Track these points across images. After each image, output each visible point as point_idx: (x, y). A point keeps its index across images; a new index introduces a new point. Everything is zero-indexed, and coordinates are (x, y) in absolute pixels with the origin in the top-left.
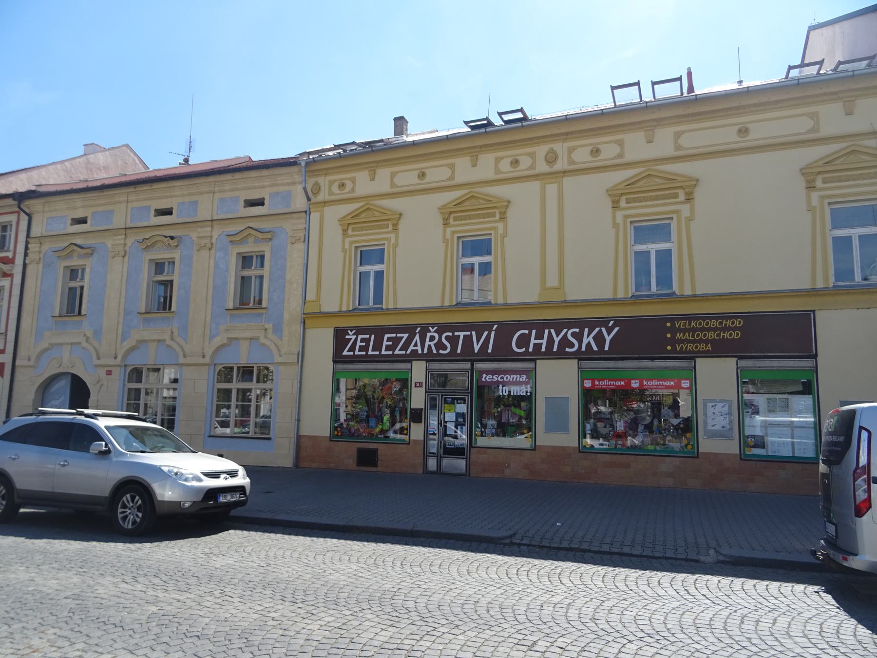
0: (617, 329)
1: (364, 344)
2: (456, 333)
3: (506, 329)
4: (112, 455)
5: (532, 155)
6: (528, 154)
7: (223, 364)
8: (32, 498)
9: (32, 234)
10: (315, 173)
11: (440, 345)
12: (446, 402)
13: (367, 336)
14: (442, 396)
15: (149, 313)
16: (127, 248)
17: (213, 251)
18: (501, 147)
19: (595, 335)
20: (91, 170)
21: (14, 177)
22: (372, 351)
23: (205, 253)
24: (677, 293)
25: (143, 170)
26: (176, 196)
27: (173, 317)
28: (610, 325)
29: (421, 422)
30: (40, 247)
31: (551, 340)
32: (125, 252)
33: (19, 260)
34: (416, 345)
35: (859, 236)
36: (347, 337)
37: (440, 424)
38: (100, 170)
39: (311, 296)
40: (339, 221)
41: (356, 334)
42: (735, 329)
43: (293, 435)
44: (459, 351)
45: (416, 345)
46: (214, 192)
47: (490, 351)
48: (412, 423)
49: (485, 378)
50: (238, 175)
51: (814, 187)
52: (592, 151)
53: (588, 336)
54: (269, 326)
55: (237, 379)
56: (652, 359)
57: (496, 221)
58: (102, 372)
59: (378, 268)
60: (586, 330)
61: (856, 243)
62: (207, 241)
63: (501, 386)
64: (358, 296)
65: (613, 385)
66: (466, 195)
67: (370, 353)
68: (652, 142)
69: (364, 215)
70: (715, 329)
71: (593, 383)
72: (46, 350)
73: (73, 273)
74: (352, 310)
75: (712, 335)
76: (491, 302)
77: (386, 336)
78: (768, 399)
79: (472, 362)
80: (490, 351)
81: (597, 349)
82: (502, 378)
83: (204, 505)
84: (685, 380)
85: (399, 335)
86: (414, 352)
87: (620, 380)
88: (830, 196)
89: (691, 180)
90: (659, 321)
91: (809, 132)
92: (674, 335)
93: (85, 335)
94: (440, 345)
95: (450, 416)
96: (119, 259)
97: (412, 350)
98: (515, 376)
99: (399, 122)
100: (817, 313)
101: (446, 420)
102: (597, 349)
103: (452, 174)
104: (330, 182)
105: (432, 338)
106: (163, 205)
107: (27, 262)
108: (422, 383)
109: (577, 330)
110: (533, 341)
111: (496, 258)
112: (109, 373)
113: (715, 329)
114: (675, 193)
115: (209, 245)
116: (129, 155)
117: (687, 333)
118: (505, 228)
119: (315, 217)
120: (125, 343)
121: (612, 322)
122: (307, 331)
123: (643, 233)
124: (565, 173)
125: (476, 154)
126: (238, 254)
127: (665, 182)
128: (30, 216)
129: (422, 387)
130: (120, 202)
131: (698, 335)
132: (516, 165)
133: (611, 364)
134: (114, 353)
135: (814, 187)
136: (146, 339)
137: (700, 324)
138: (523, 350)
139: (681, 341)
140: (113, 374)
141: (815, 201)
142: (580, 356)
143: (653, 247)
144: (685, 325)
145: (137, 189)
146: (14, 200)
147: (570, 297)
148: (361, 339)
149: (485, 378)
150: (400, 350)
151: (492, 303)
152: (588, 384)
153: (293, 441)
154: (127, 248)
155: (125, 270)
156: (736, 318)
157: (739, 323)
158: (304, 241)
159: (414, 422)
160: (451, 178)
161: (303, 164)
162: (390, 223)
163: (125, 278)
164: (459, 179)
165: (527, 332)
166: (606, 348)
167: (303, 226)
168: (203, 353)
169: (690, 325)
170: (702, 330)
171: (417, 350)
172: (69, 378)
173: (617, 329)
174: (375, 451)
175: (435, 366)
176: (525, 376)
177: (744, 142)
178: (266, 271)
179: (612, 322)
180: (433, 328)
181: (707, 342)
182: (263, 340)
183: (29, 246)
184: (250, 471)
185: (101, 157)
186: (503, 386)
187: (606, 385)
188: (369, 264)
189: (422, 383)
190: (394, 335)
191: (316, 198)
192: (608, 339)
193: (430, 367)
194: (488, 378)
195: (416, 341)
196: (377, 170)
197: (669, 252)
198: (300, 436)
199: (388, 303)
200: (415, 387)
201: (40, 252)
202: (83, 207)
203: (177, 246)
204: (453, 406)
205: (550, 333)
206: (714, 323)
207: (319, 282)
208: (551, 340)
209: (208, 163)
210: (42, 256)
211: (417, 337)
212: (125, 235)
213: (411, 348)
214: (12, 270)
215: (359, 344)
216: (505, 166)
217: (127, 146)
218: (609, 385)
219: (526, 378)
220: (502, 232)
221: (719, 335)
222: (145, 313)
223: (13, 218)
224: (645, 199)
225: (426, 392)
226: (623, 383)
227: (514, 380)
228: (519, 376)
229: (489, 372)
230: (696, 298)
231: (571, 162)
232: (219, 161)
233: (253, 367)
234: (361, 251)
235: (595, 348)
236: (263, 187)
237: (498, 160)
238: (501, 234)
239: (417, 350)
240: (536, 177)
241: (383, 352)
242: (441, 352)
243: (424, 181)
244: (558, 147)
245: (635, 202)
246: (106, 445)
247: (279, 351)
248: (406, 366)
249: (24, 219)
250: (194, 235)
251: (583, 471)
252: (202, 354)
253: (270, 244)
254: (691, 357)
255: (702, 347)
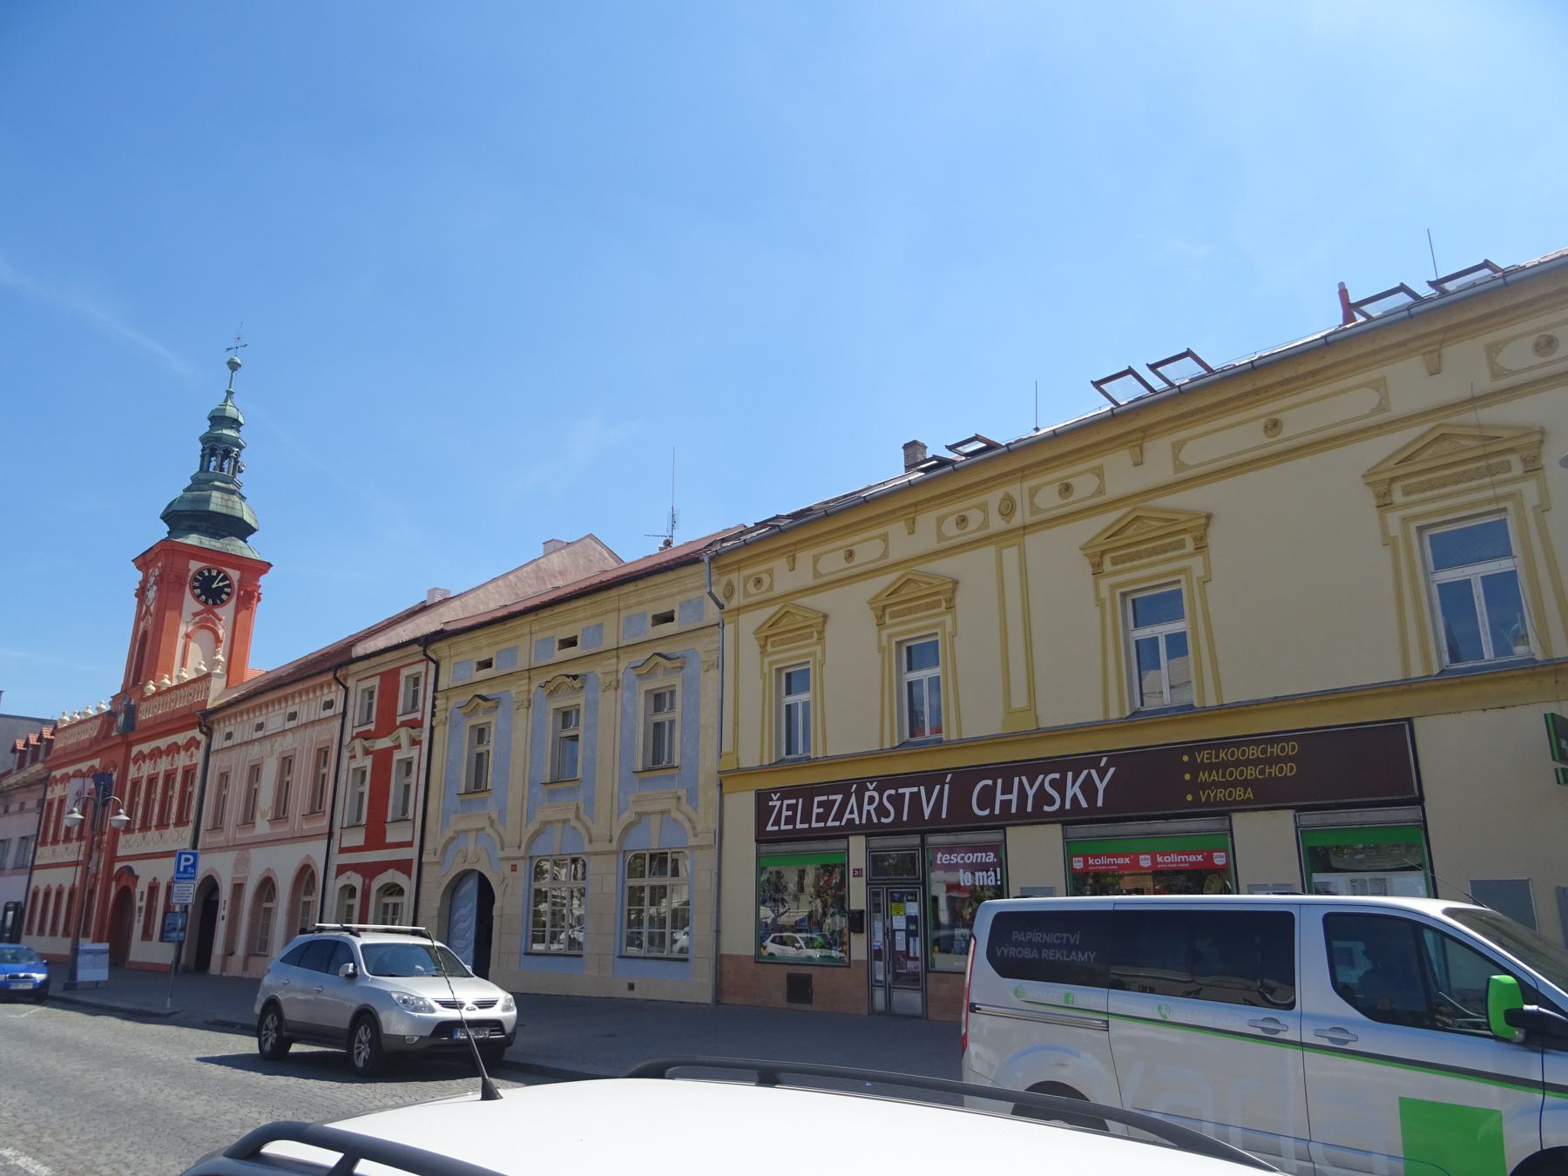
0: (1112, 770)
1: (790, 813)
2: (901, 791)
3: (964, 778)
4: (358, 979)
5: (983, 508)
6: (1091, 471)
7: (633, 851)
8: (309, 1033)
9: (440, 689)
10: (723, 569)
11: (881, 811)
12: (893, 900)
13: (794, 801)
14: (887, 889)
15: (556, 782)
16: (531, 696)
17: (619, 691)
18: (1180, 422)
19: (1082, 783)
20: (543, 579)
21: (445, 608)
23: (611, 694)
24: (1196, 704)
25: (615, 565)
26: (580, 620)
27: (578, 786)
28: (1102, 764)
29: (862, 932)
30: (447, 703)
31: (1023, 795)
32: (529, 701)
33: (427, 724)
34: (852, 812)
35: (1167, 636)
36: (771, 803)
37: (886, 934)
38: (555, 577)
40: (1363, 476)
41: (781, 799)
42: (1287, 759)
43: (712, 955)
44: (905, 818)
45: (852, 812)
46: (619, 610)
47: (944, 816)
48: (852, 934)
49: (941, 859)
50: (641, 584)
51: (1390, 504)
52: (1266, 428)
53: (1073, 785)
54: (682, 793)
55: (650, 872)
56: (1166, 818)
57: (941, 614)
58: (507, 868)
60: (1070, 774)
61: (1478, 591)
62: (525, 697)
64: (784, 740)
65: (1186, 862)
67: (799, 826)
69: (785, 620)
70: (1255, 762)
71: (1086, 862)
72: (452, 839)
73: (480, 733)
74: (1130, 716)
75: (1251, 773)
76: (1192, 705)
77: (817, 799)
78: (1352, 881)
79: (922, 834)
80: (944, 816)
82: (962, 858)
83: (435, 1041)
84: (1218, 851)
85: (831, 797)
86: (851, 821)
87: (1123, 856)
88: (1417, 517)
90: (1170, 753)
91: (1374, 412)
92: (1195, 775)
93: (490, 818)
94: (881, 811)
95: (899, 923)
96: (523, 711)
98: (979, 855)
99: (910, 451)
100: (1417, 723)
101: (894, 928)
103: (1100, 483)
104: (1030, 489)
105: (871, 800)
106: (566, 633)
107: (434, 724)
109: (1057, 776)
110: (999, 797)
112: (514, 868)
113: (1255, 762)
114: (1180, 540)
115: (614, 683)
116: (595, 549)
117: (1214, 772)
118: (1207, 567)
119: (729, 629)
120: (530, 826)
121: (1104, 760)
122: (727, 798)
123: (1450, 549)
124: (1025, 528)
125: (1140, 442)
126: (647, 692)
127: (1165, 524)
128: (437, 664)
129: (861, 876)
130: (523, 635)
131: (1231, 774)
132: (964, 524)
133: (1108, 829)
134: (518, 840)
135: (1390, 504)
136: (550, 819)
137: (1233, 754)
138: (987, 812)
139: (1206, 786)
140: (518, 869)
141: (1395, 529)
142: (1067, 818)
143: (1475, 573)
144: (1210, 758)
145: (555, 611)
146: (420, 646)
147: (1045, 723)
148: (819, 802)
149: (941, 859)
151: (944, 739)
152: (1078, 864)
153: (713, 961)
154: (531, 696)
155: (530, 725)
156: (1287, 739)
157: (1291, 749)
158: (718, 667)
159: (854, 932)
160: (885, 555)
161: (706, 559)
162: (813, 629)
163: (529, 737)
164: (1114, 491)
165: (989, 782)
166: (1100, 804)
167: (715, 646)
168: (611, 836)
169: (1217, 756)
170: (1237, 764)
171: (854, 819)
172: (477, 876)
173: (1112, 770)
174: (809, 977)
175: (877, 842)
176: (992, 854)
177: (966, 534)
178: (677, 715)
179: (1104, 760)
180: (871, 783)
181: (1245, 784)
182: (675, 814)
183: (437, 703)
184: (521, 1000)
185: (556, 560)
187: (1104, 865)
188: (798, 693)
189: (862, 870)
190: (825, 798)
191: (729, 603)
192: (1101, 787)
193: (871, 845)
194: (944, 858)
196: (797, 555)
197: (1511, 576)
198: (722, 956)
200: (854, 876)
201: (446, 710)
202: (488, 645)
203: (582, 687)
204: (901, 905)
205: (1021, 783)
206: (1253, 752)
207: (736, 724)
208: (1023, 795)
209: (682, 546)
210: (448, 715)
211: (853, 800)
212: (530, 678)
213: (847, 816)
214: (420, 736)
215: (785, 813)
216: (950, 528)
217: (591, 536)
218: (1177, 863)
219: (994, 857)
220: (1536, 501)
221: (1262, 772)
222: (643, 771)
223: (421, 668)
224: (1139, 555)
225: (867, 884)
226: (1200, 858)
227: (979, 861)
228: (984, 854)
230: (1260, 707)
231: (1035, 509)
232: (695, 541)
233: (667, 853)
234: (1133, 601)
235: (1084, 805)
236: (671, 596)
237: (940, 520)
238: (1198, 578)
239: (854, 819)
240: (987, 540)
241: (814, 825)
242: (883, 820)
243: (1280, 437)
244: (1015, 490)
245: (1124, 562)
246: (355, 967)
247: (694, 828)
248: (838, 844)
249: (432, 666)
250: (599, 671)
252: (608, 838)
253: (681, 674)
254: (1224, 811)
255: (1239, 793)
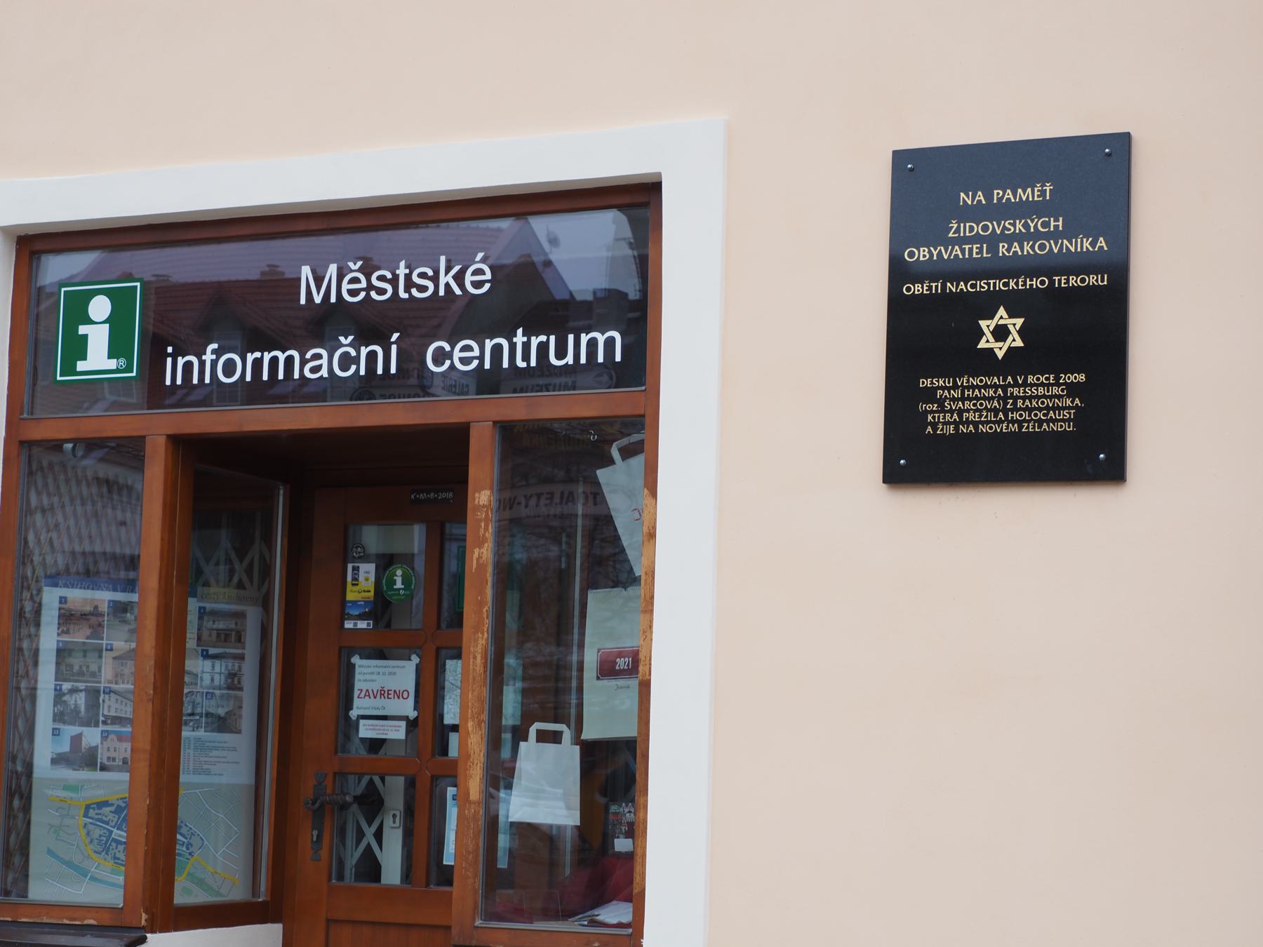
22: (60, 376)
36: (951, 225)
67: (985, 255)
81: (461, 293)
97: (1007, 198)
102: (461, 293)
150: (953, 234)
195: (318, 293)
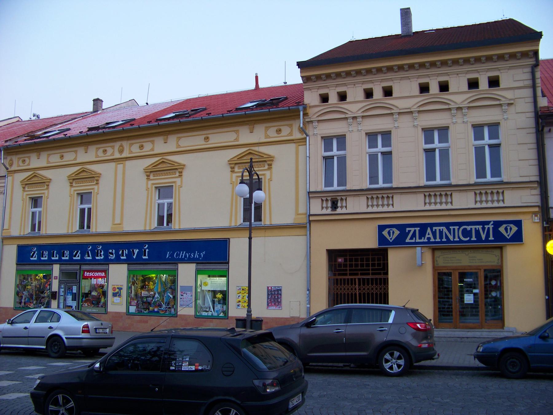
14: (66, 284)
39: (6, 227)
59: (170, 201)
63: (93, 278)
66: (31, 175)
68: (252, 132)
89: (270, 157)
98: (99, 273)
108: (57, 277)
111: (93, 206)
118: (48, 193)
124: (127, 159)
158: (4, 194)
186: (94, 279)
189: (57, 277)
195: (445, 233)
199: (43, 232)
200: (54, 279)
219: (105, 274)
225: (59, 282)
227: (99, 275)
228: (101, 273)
229: (88, 271)
251: (128, 325)
